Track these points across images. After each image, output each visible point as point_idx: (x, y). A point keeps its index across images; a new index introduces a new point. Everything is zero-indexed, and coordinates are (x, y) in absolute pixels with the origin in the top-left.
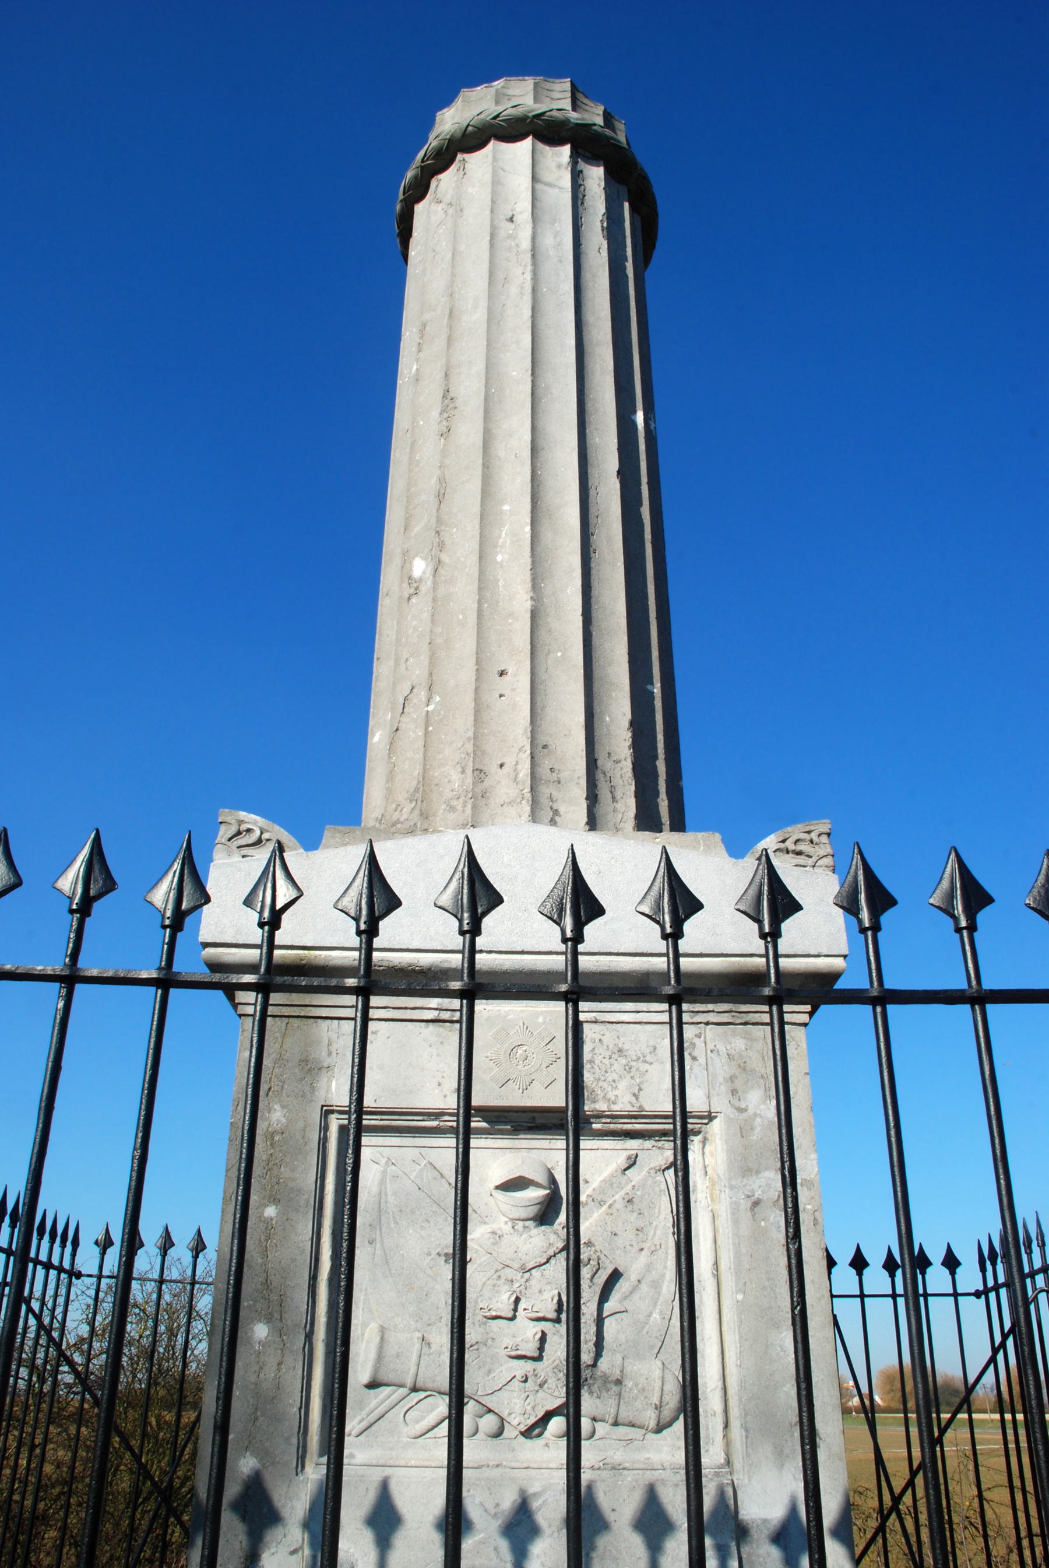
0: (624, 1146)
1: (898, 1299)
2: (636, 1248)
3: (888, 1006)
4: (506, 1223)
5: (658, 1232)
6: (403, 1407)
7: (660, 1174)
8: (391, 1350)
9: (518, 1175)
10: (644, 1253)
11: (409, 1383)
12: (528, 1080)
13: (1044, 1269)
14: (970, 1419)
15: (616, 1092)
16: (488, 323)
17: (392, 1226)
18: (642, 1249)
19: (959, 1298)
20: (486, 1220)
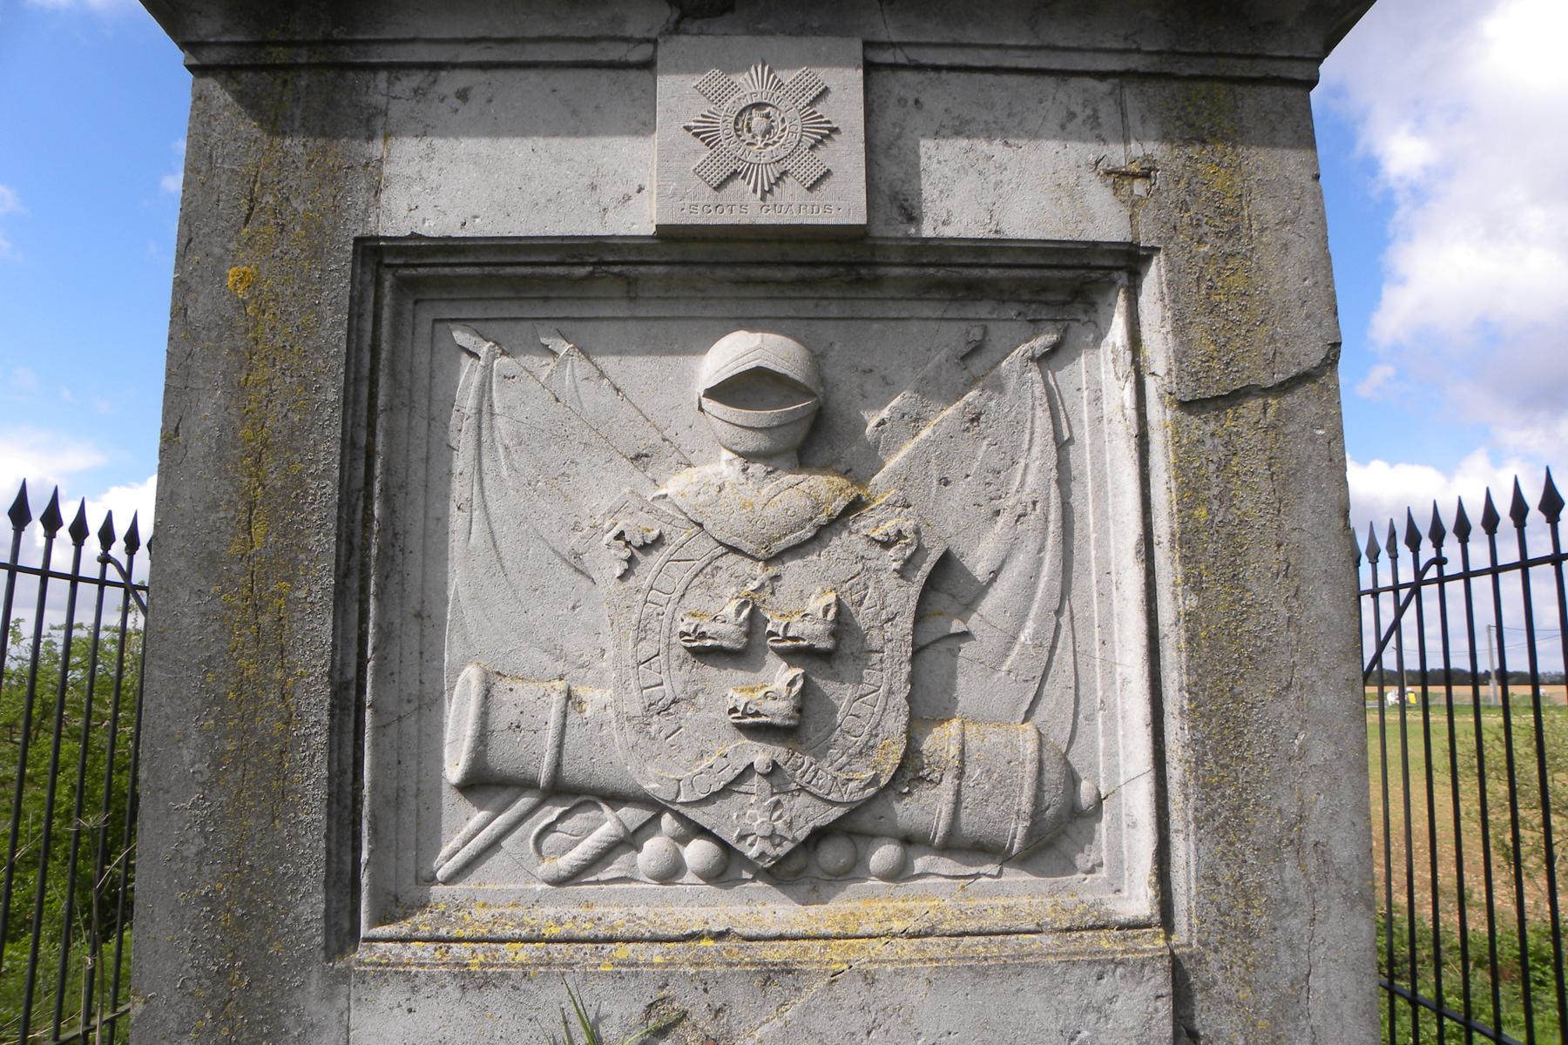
0: (962, 314)
1: (1525, 667)
2: (986, 510)
3: (1442, 667)
4: (730, 462)
5: (1030, 479)
6: (534, 825)
7: (1033, 366)
8: (502, 717)
9: (753, 365)
10: (1001, 520)
11: (543, 777)
12: (774, 172)
13: (1556, 559)
14: (1505, 696)
15: (948, 203)
16: (1328, 257)
17: (505, 473)
18: (998, 513)
19: (69, 571)
20: (692, 458)
